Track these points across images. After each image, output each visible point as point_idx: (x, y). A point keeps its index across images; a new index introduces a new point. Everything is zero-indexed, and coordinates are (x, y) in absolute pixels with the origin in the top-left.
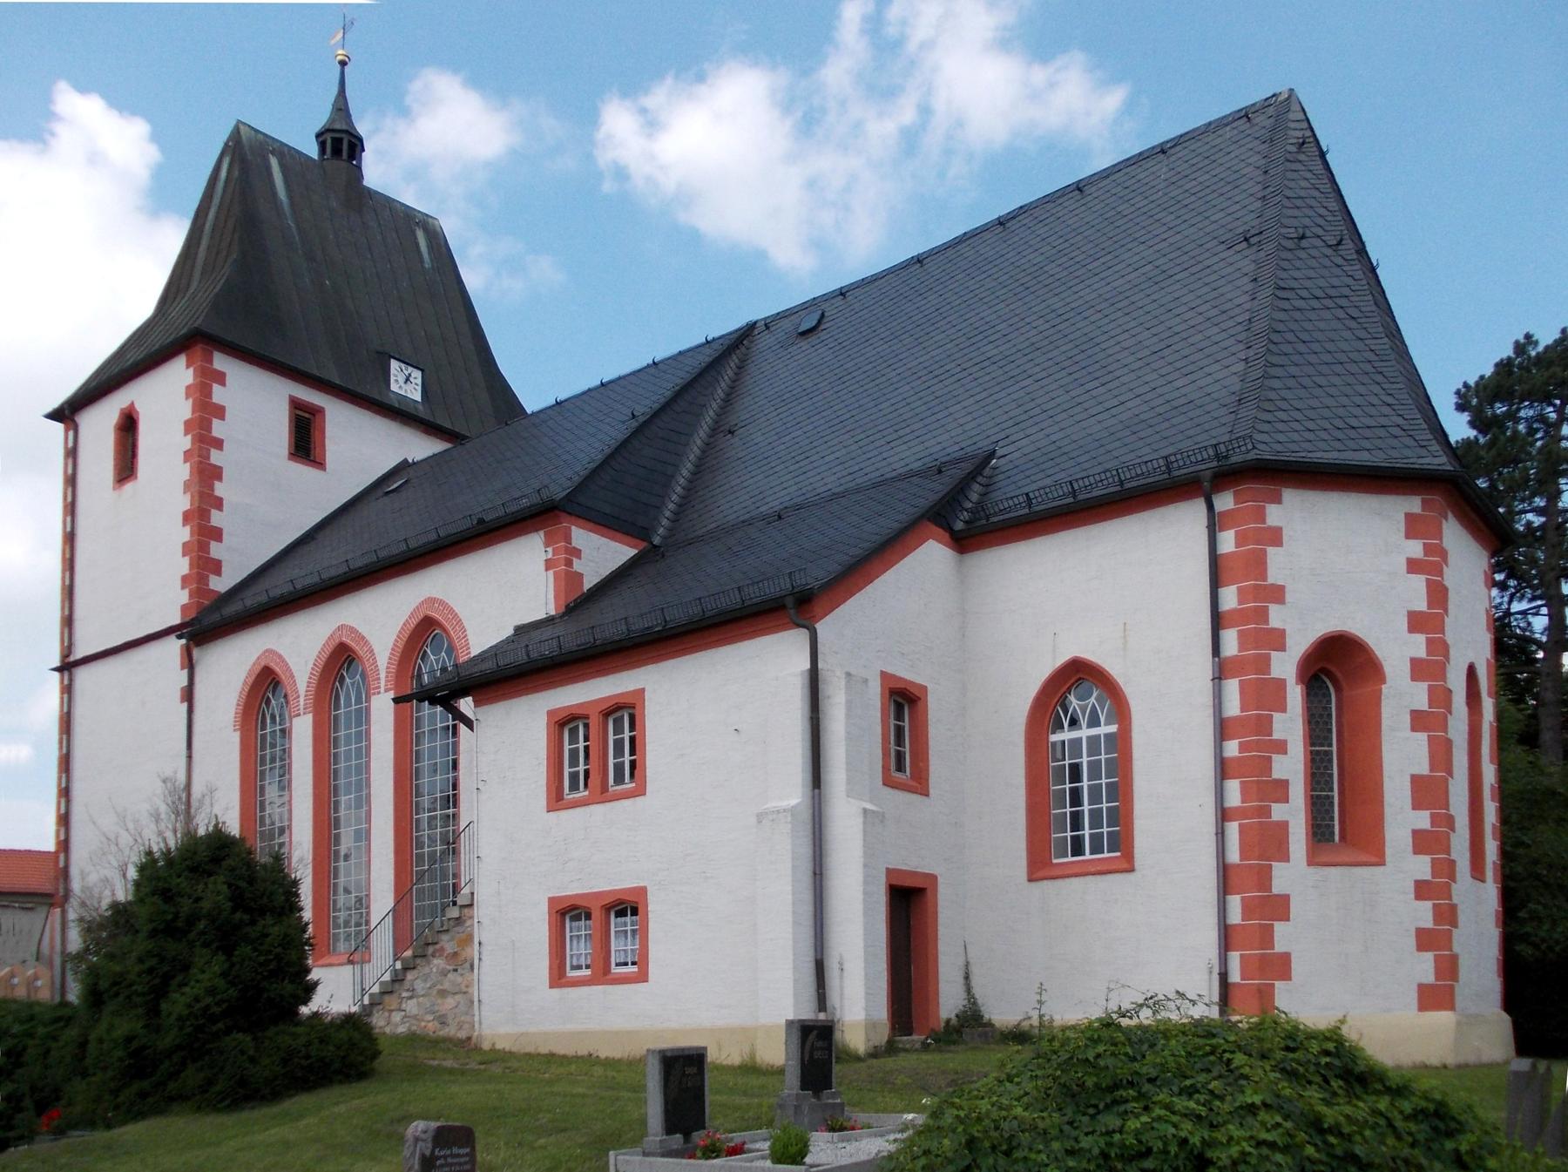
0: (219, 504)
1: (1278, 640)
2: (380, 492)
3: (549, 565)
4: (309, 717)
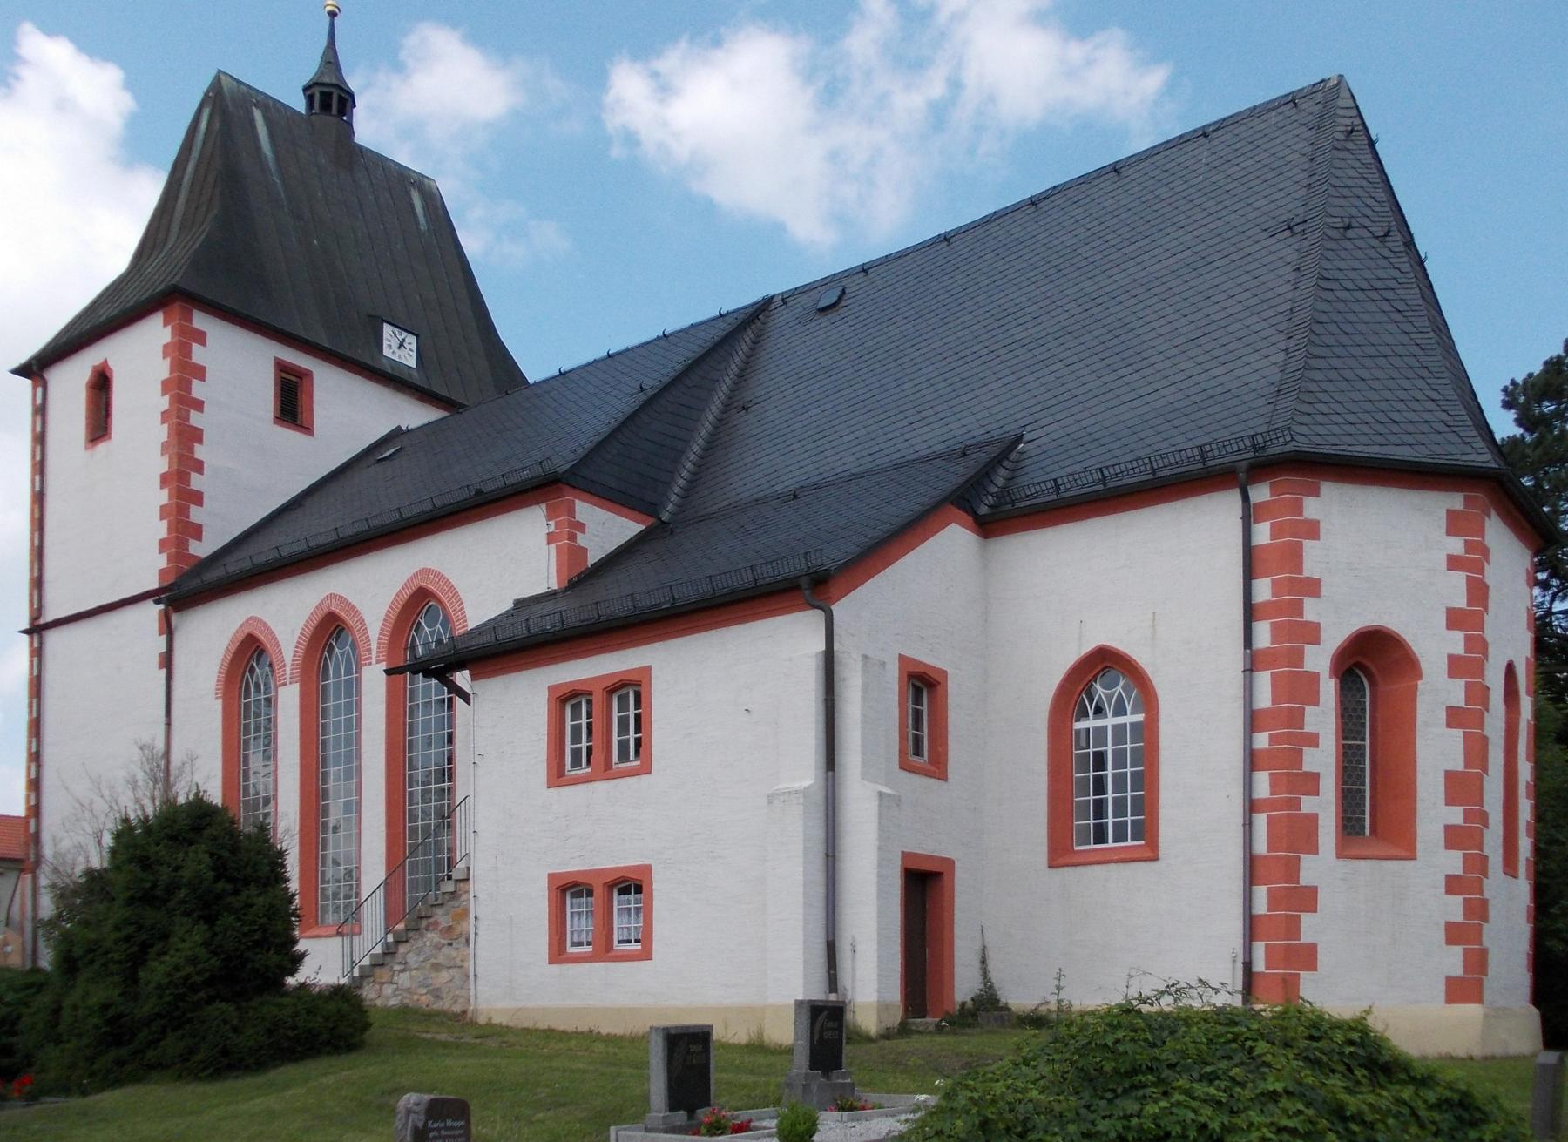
1: (1312, 633)
2: (371, 460)
3: (551, 538)
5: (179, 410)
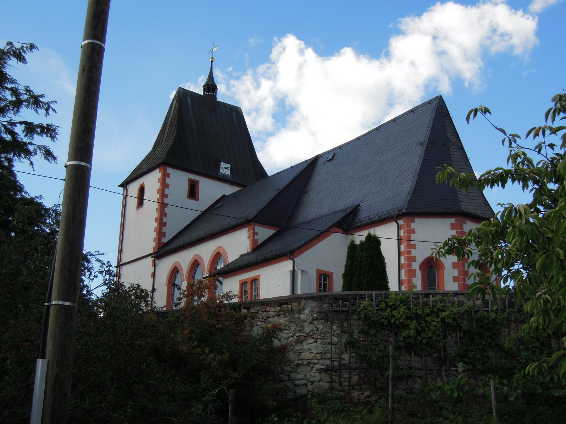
0: (166, 215)
1: (414, 259)
3: (249, 237)
4: (186, 282)
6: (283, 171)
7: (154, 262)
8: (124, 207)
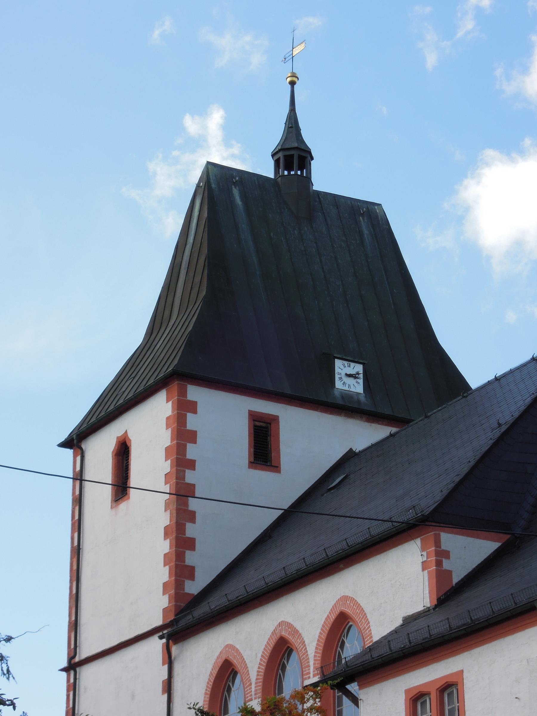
0: (192, 517)
3: (425, 566)
5: (177, 471)
6: (511, 372)
7: (168, 650)
8: (78, 501)
